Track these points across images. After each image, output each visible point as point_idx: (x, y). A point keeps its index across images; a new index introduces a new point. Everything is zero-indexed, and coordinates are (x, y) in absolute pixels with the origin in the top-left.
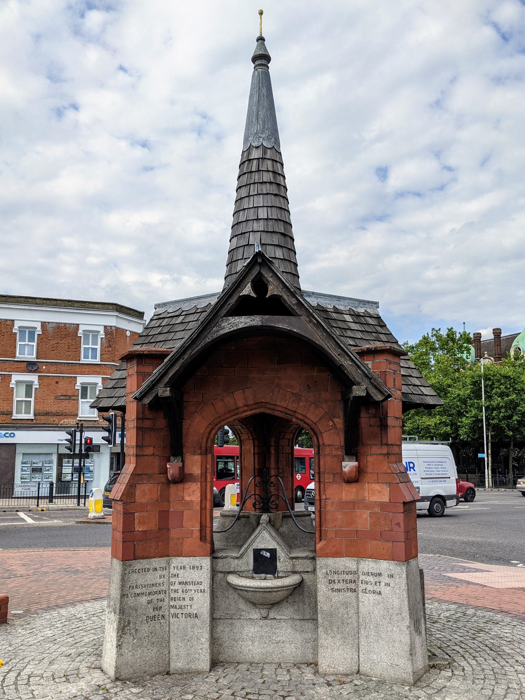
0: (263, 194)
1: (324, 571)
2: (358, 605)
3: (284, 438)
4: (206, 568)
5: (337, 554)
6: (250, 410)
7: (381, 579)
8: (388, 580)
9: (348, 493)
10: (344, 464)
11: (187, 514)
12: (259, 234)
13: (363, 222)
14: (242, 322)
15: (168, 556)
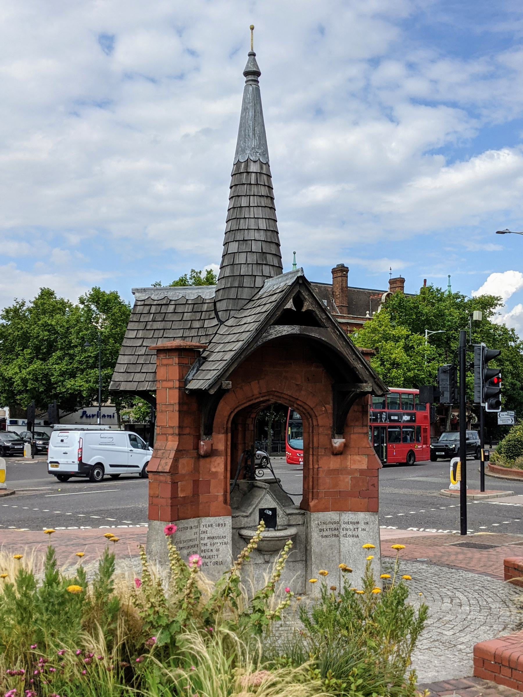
0: (262, 207)
1: (316, 522)
2: (340, 546)
3: (249, 418)
4: (229, 525)
5: (326, 509)
6: (262, 397)
7: (359, 526)
8: (364, 526)
9: (334, 463)
10: (335, 440)
11: (213, 482)
12: (260, 242)
13: (78, 106)
14: (285, 330)
15: (199, 517)
